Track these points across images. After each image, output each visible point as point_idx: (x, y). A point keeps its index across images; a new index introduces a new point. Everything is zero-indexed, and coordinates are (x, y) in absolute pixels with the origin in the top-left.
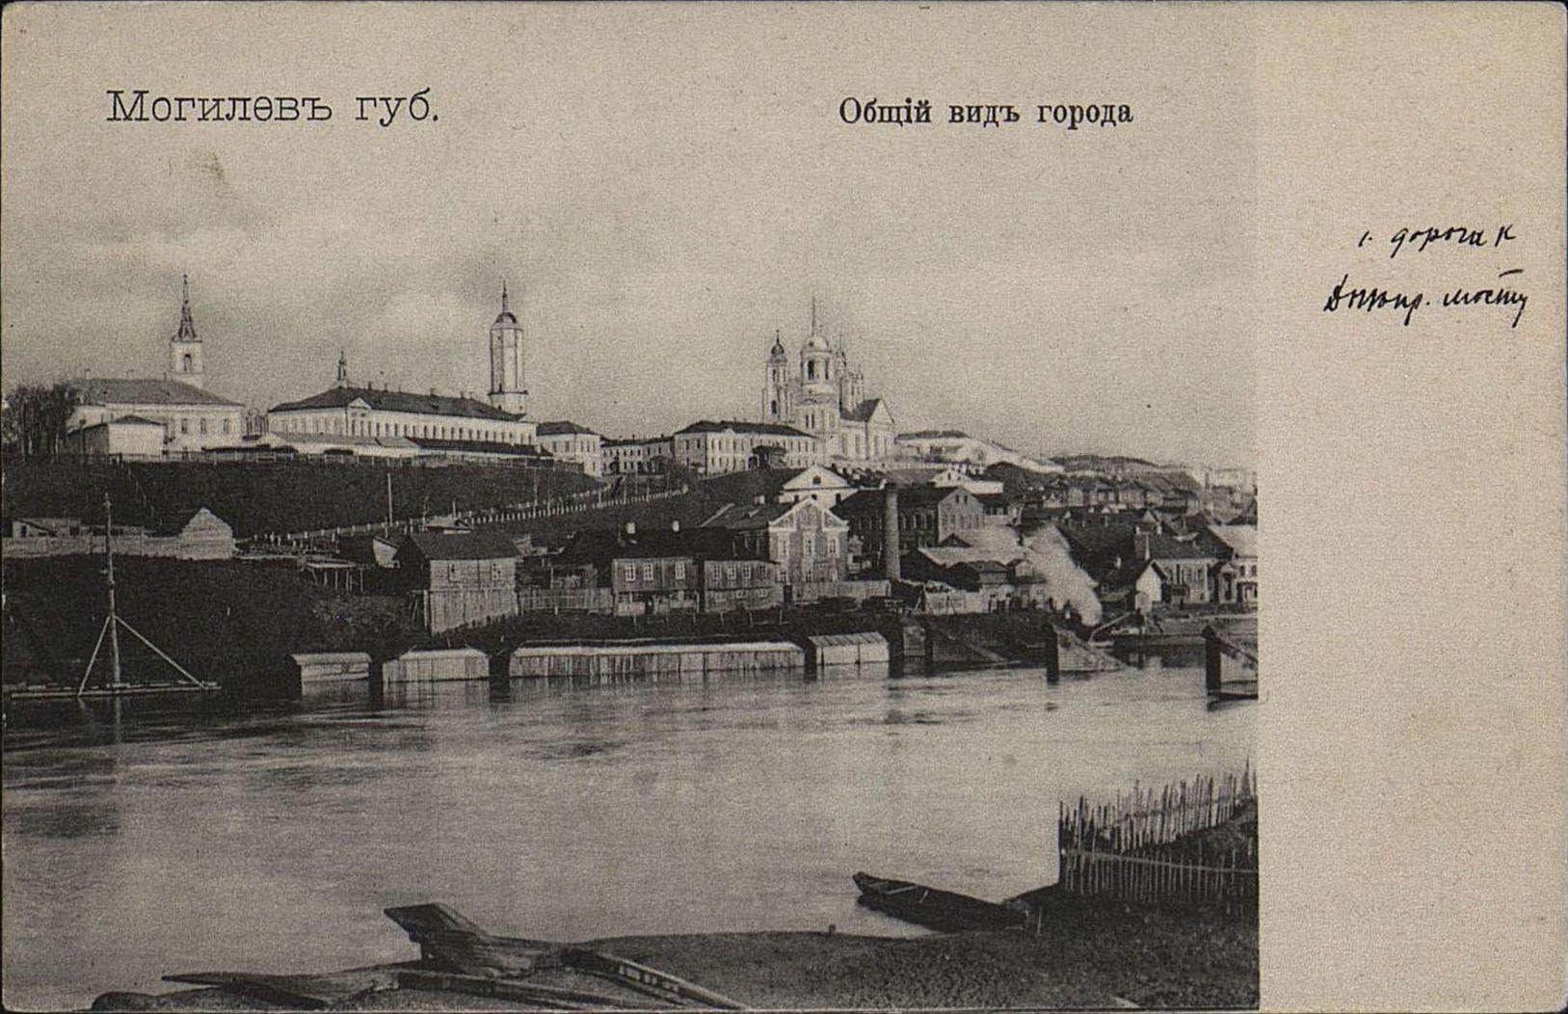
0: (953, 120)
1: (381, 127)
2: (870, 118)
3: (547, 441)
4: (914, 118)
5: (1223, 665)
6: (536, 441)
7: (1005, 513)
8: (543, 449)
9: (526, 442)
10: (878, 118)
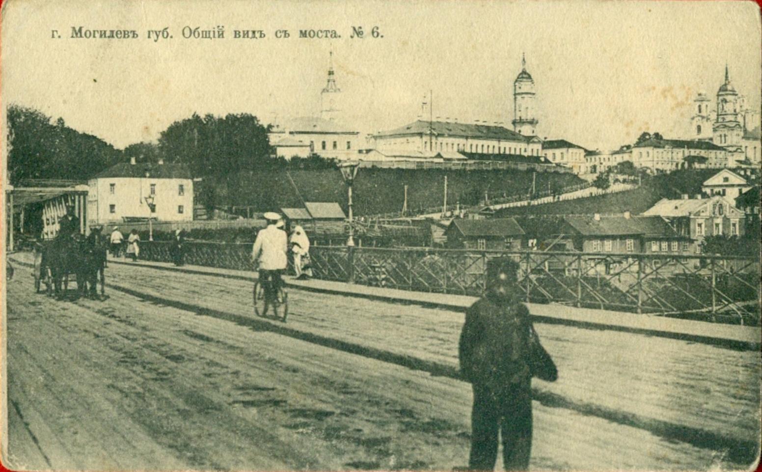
0: (235, 37)
1: (275, 37)
2: (165, 36)
3: (549, 153)
5: (535, 413)
6: (542, 153)
7: (591, 194)
8: (545, 158)
9: (535, 154)
10: (201, 36)
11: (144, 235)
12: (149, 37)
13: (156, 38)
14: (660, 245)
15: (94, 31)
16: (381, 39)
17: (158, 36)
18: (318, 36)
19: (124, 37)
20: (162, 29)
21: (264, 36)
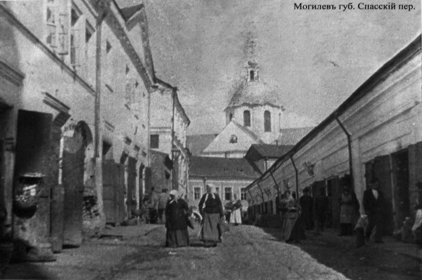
4: (391, 7)
11: (191, 177)
12: (340, 8)
13: (344, 9)
14: (339, 121)
15: (309, 6)
16: (354, 10)
17: (345, 8)
18: (405, 8)
19: (327, 8)
20: (348, 4)
21: (335, 8)
